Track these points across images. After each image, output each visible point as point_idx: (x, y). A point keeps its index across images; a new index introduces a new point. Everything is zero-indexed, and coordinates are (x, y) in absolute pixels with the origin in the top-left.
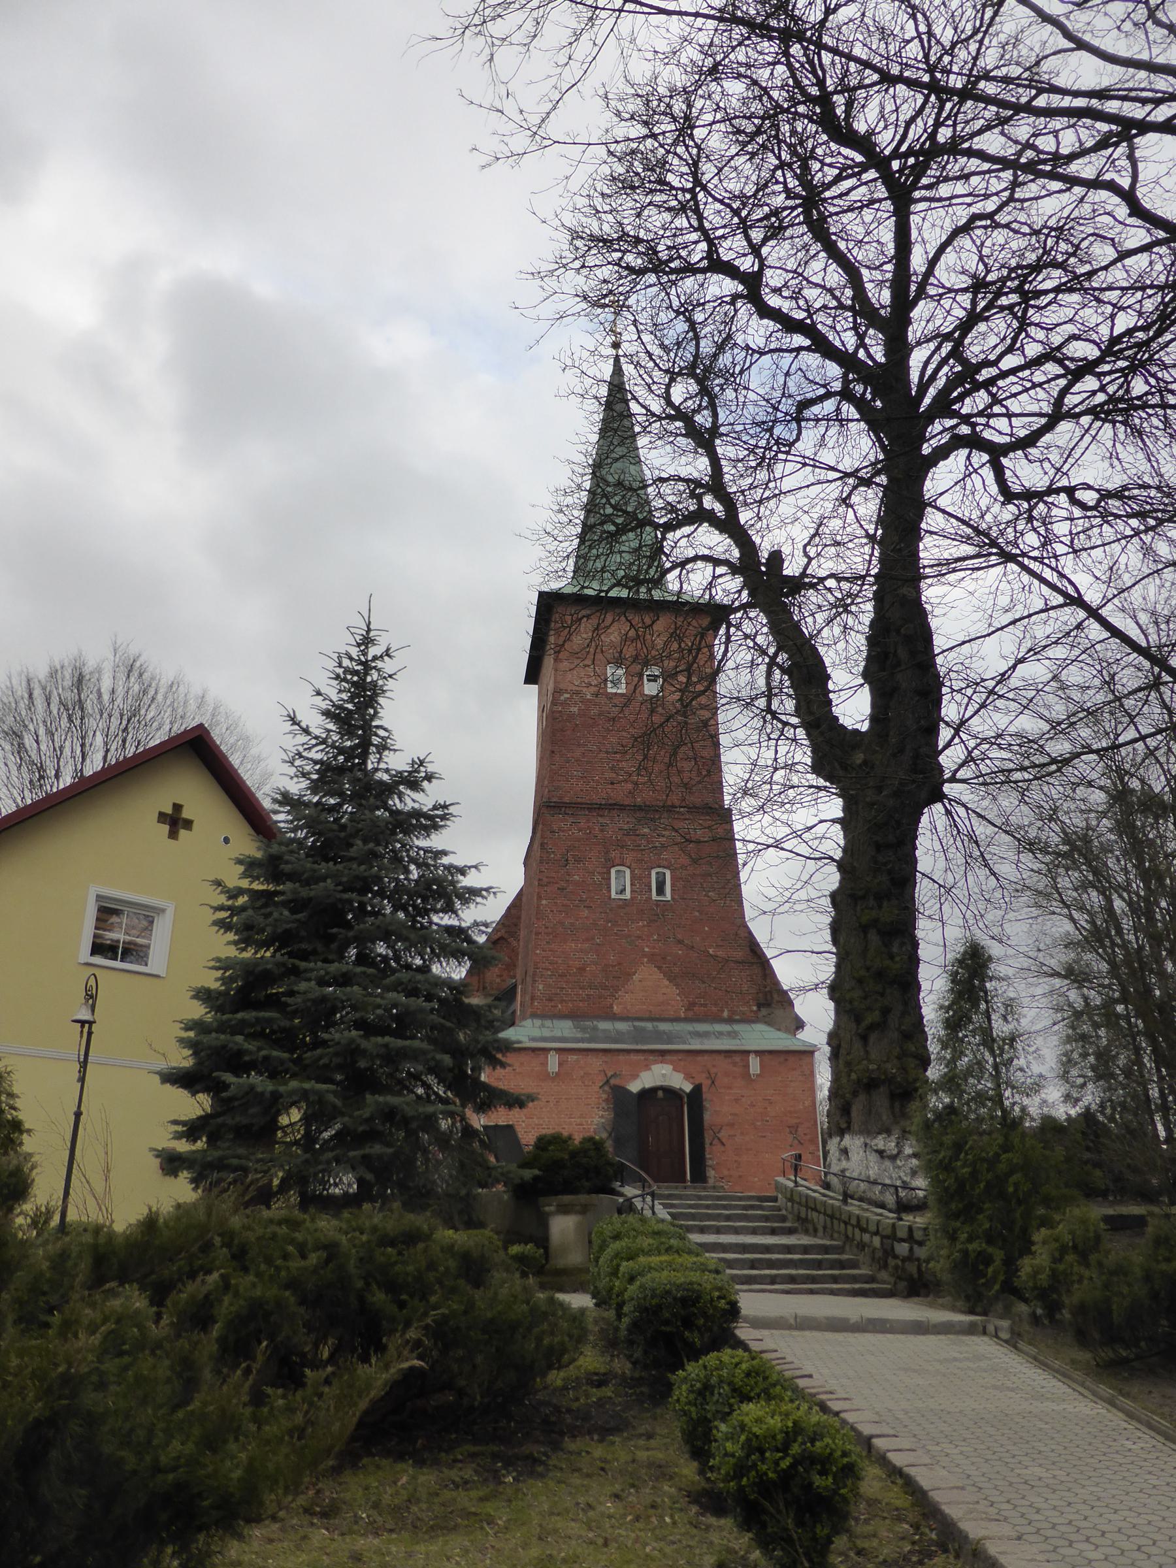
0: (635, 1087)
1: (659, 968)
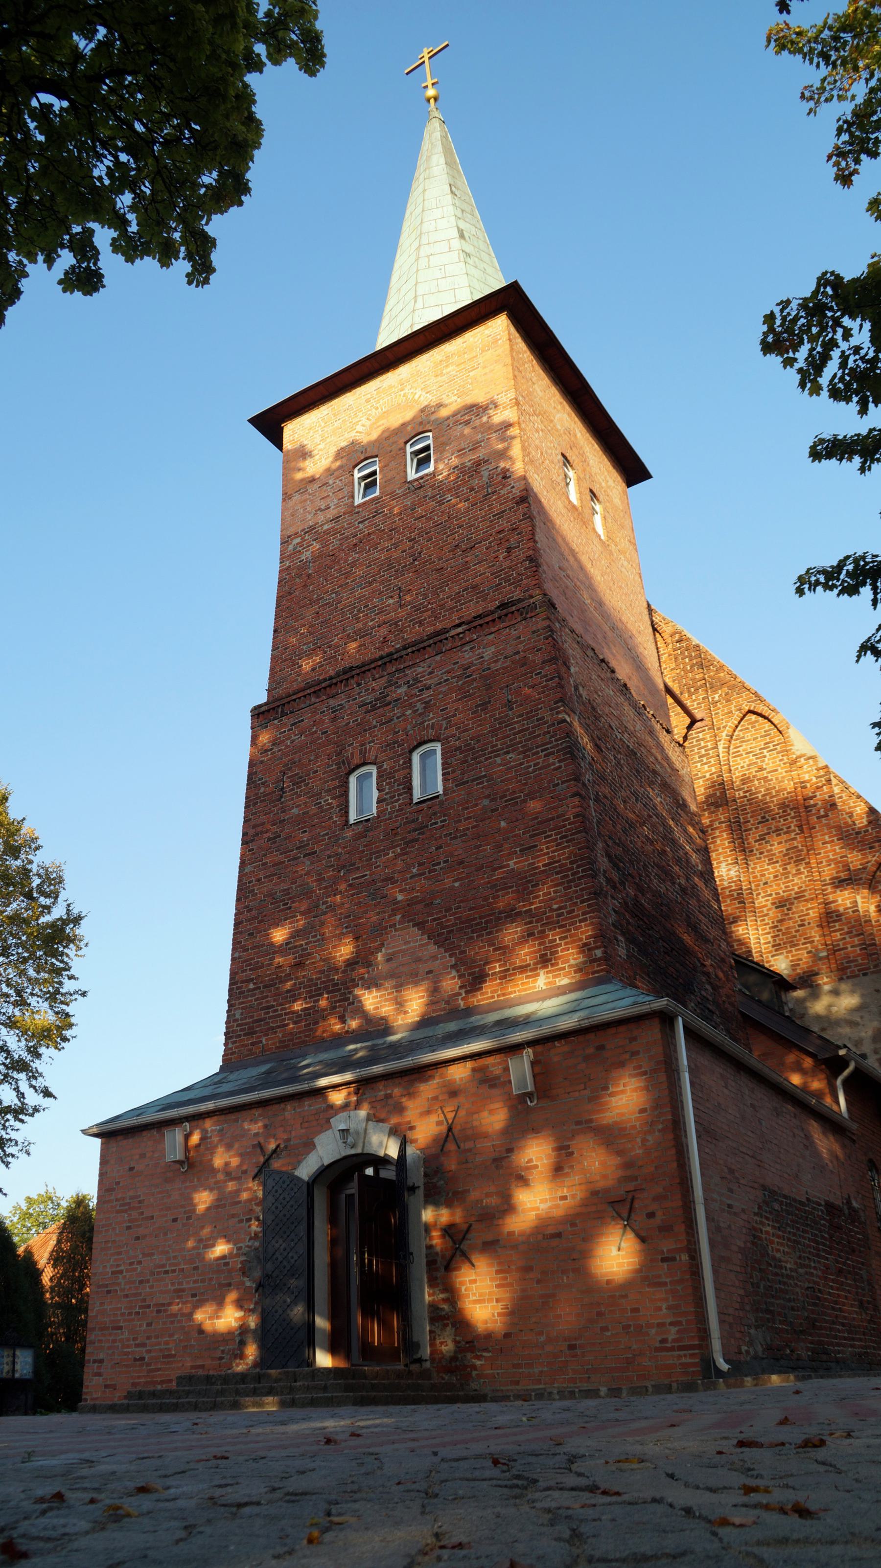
0: (306, 1170)
1: (420, 925)
